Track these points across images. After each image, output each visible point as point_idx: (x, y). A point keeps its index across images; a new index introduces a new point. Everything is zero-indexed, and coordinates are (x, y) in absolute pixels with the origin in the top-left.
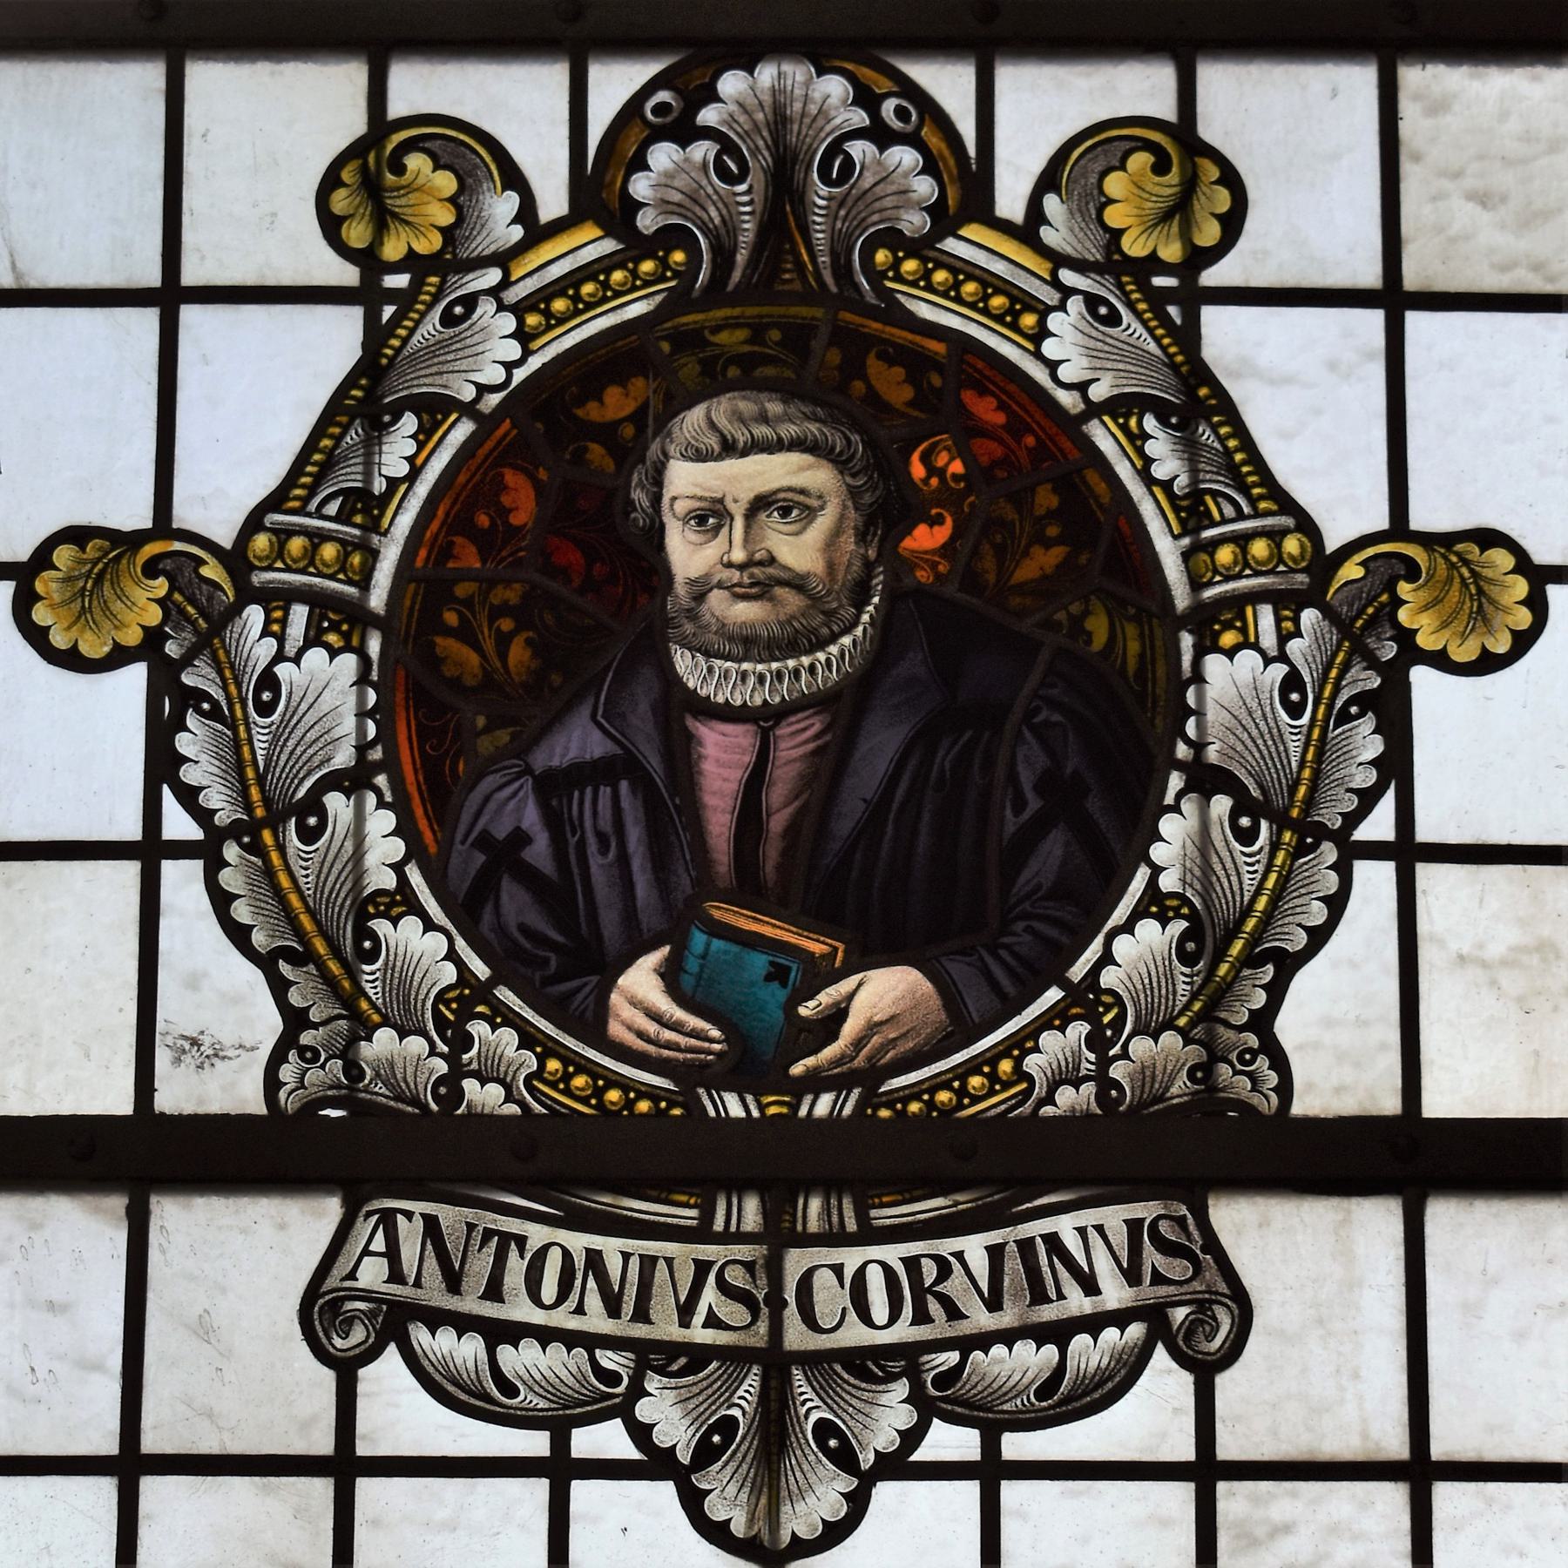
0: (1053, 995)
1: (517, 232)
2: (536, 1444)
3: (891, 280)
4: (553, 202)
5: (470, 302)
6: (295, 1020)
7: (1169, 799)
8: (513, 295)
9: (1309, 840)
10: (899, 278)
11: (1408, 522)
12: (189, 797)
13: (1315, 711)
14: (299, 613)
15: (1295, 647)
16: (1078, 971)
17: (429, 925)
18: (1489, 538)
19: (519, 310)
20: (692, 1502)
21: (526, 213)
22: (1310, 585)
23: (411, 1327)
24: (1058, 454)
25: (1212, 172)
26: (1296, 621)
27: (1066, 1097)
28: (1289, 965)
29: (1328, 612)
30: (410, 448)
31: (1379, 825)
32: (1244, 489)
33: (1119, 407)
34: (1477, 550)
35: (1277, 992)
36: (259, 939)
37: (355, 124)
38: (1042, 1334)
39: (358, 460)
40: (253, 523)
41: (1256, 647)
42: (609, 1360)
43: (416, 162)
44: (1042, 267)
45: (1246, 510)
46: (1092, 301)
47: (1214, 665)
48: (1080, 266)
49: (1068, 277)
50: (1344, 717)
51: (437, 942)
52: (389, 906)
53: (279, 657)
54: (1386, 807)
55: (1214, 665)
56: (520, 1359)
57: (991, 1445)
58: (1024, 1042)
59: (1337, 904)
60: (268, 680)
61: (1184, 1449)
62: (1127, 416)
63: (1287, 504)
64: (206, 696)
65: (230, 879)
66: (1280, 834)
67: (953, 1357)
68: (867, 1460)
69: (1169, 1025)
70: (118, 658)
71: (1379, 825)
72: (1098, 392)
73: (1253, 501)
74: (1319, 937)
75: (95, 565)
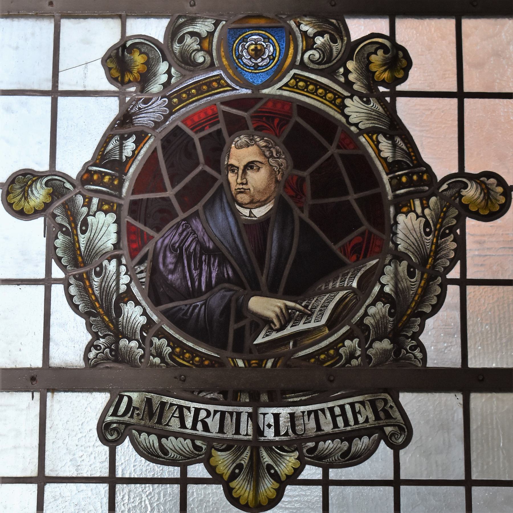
2: (174, 472)
12: (59, 260)
14: (95, 201)
16: (357, 317)
20: (229, 493)
25: (401, 54)
28: (426, 316)
30: (133, 146)
33: (370, 132)
39: (117, 150)
41: (415, 211)
42: (198, 443)
47: (401, 218)
53: (88, 215)
54: (457, 267)
55: (401, 218)
56: (170, 443)
57: (326, 474)
59: (441, 298)
60: (85, 223)
62: (373, 134)
64: (64, 226)
70: (36, 213)
71: (455, 273)
74: (436, 309)
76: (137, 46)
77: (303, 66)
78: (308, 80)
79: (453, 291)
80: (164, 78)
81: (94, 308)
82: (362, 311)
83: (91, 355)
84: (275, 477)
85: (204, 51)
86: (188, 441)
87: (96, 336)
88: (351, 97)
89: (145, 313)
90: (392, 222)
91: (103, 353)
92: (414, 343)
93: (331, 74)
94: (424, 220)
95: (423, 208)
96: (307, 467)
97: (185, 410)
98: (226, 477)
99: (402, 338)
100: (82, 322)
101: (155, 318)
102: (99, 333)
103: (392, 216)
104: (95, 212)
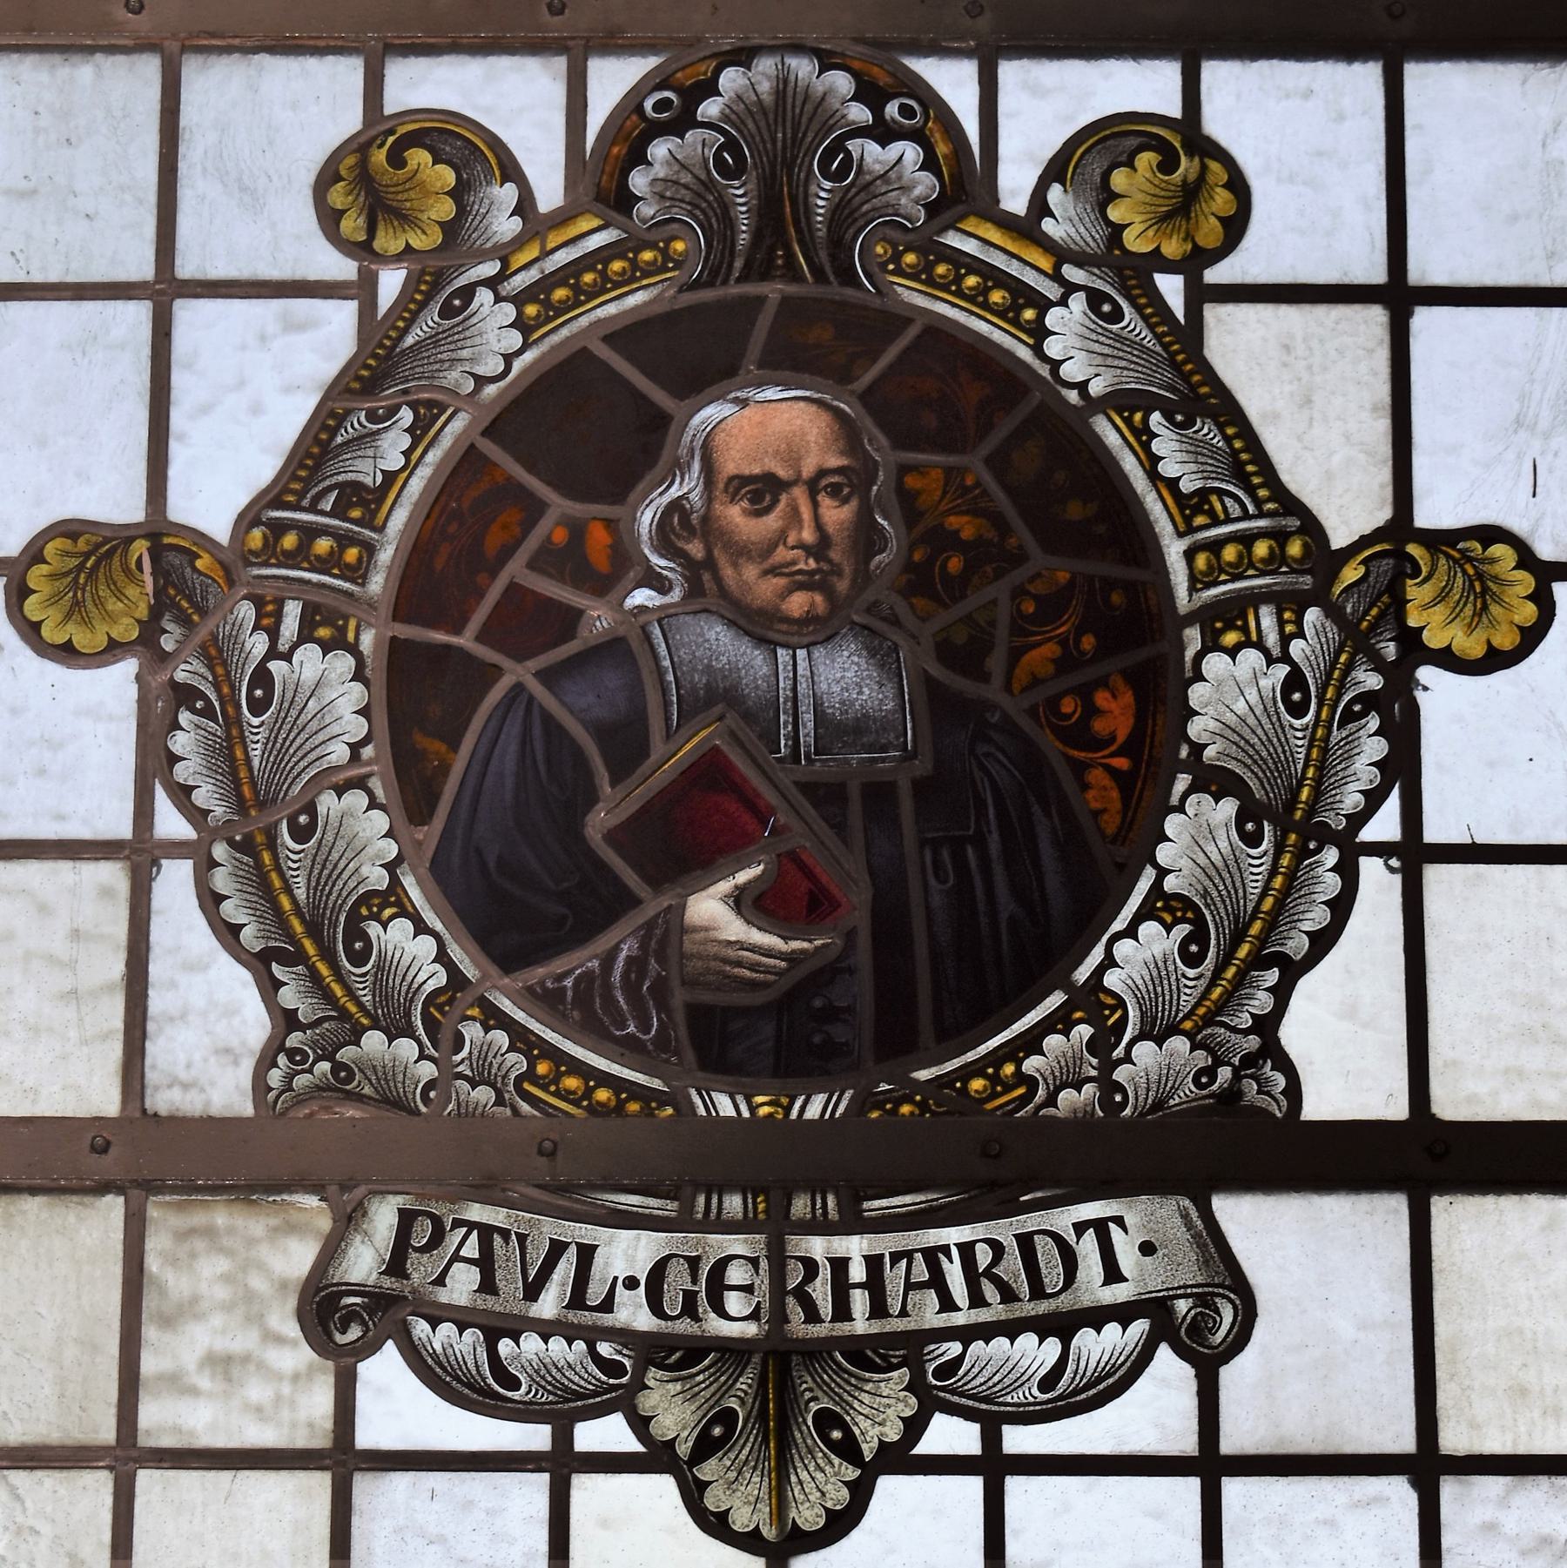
0: (1056, 1000)
1: (516, 224)
2: (536, 1437)
3: (893, 273)
4: (549, 192)
5: (468, 293)
6: (287, 1020)
7: (1175, 800)
8: (509, 287)
10: (899, 272)
11: (1412, 520)
12: (182, 795)
13: (1318, 713)
14: (293, 610)
15: (1297, 648)
16: (1082, 974)
17: (421, 928)
18: (1490, 534)
19: (519, 300)
20: (693, 1496)
21: (525, 205)
24: (1206, 1289)
26: (1299, 622)
27: (1067, 1097)
28: (1293, 971)
29: (1333, 612)
31: (1385, 825)
32: (1251, 490)
33: (1121, 402)
34: (1479, 546)
35: (1282, 994)
36: (248, 935)
37: (351, 121)
38: (1044, 1327)
40: (248, 519)
41: (1260, 645)
42: (605, 1349)
43: (419, 157)
44: (1045, 263)
45: (1251, 509)
46: (1095, 299)
48: (1081, 260)
49: (1072, 273)
50: (1349, 717)
51: (427, 945)
52: (382, 908)
53: (272, 653)
54: (1392, 804)
55: (1215, 664)
57: (991, 1438)
58: (1031, 1043)
59: (1342, 907)
60: (262, 677)
63: (1291, 504)
64: (202, 696)
66: (1285, 836)
68: (868, 1451)
69: (1173, 1030)
70: (113, 651)
71: (1385, 825)
72: (1096, 388)
73: (1258, 503)
74: (1323, 942)
75: (87, 559)
81: (291, 937)
82: (1097, 955)
83: (275, 1077)
89: (442, 957)
90: (1189, 674)
97: (497, 1240)
101: (470, 972)
103: (1190, 654)
104: (294, 647)
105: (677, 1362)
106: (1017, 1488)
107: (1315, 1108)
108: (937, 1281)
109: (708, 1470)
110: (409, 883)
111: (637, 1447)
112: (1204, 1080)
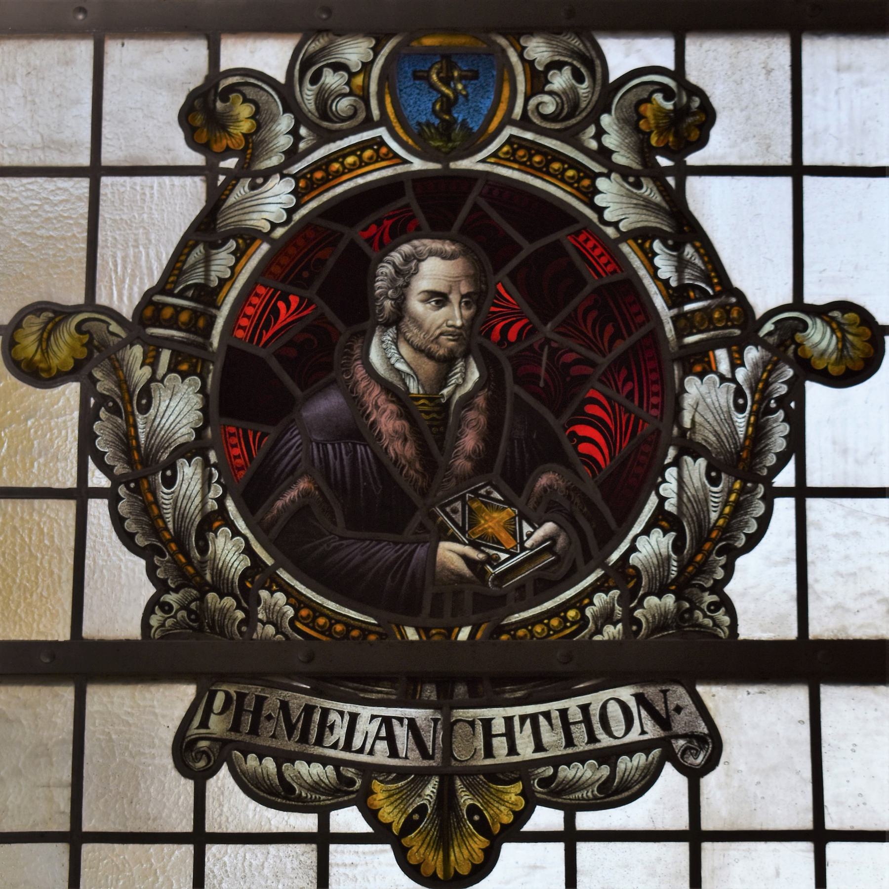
2: (308, 822)
9: (749, 485)
15: (741, 374)
16: (615, 556)
22: (759, 336)
23: (775, 485)
30: (232, 261)
36: (140, 541)
41: (716, 372)
42: (349, 773)
53: (153, 379)
57: (570, 820)
59: (764, 522)
61: (682, 823)
62: (644, 242)
65: (123, 507)
67: (550, 771)
68: (496, 829)
71: (786, 478)
74: (753, 541)
76: (242, 88)
77: (525, 122)
78: (533, 146)
79: (784, 508)
80: (284, 142)
83: (154, 621)
84: (483, 827)
85: (355, 95)
86: (330, 768)
87: (162, 587)
88: (608, 176)
91: (174, 617)
92: (715, 598)
93: (572, 137)
94: (733, 386)
95: (734, 366)
96: (539, 809)
98: (396, 830)
99: (695, 591)
100: (141, 564)
102: (169, 581)
104: (165, 376)
105: (393, 779)
106: (583, 849)
107: (746, 632)
108: (391, 739)
109: (412, 840)
110: (230, 505)
111: (367, 829)
112: (712, 608)
